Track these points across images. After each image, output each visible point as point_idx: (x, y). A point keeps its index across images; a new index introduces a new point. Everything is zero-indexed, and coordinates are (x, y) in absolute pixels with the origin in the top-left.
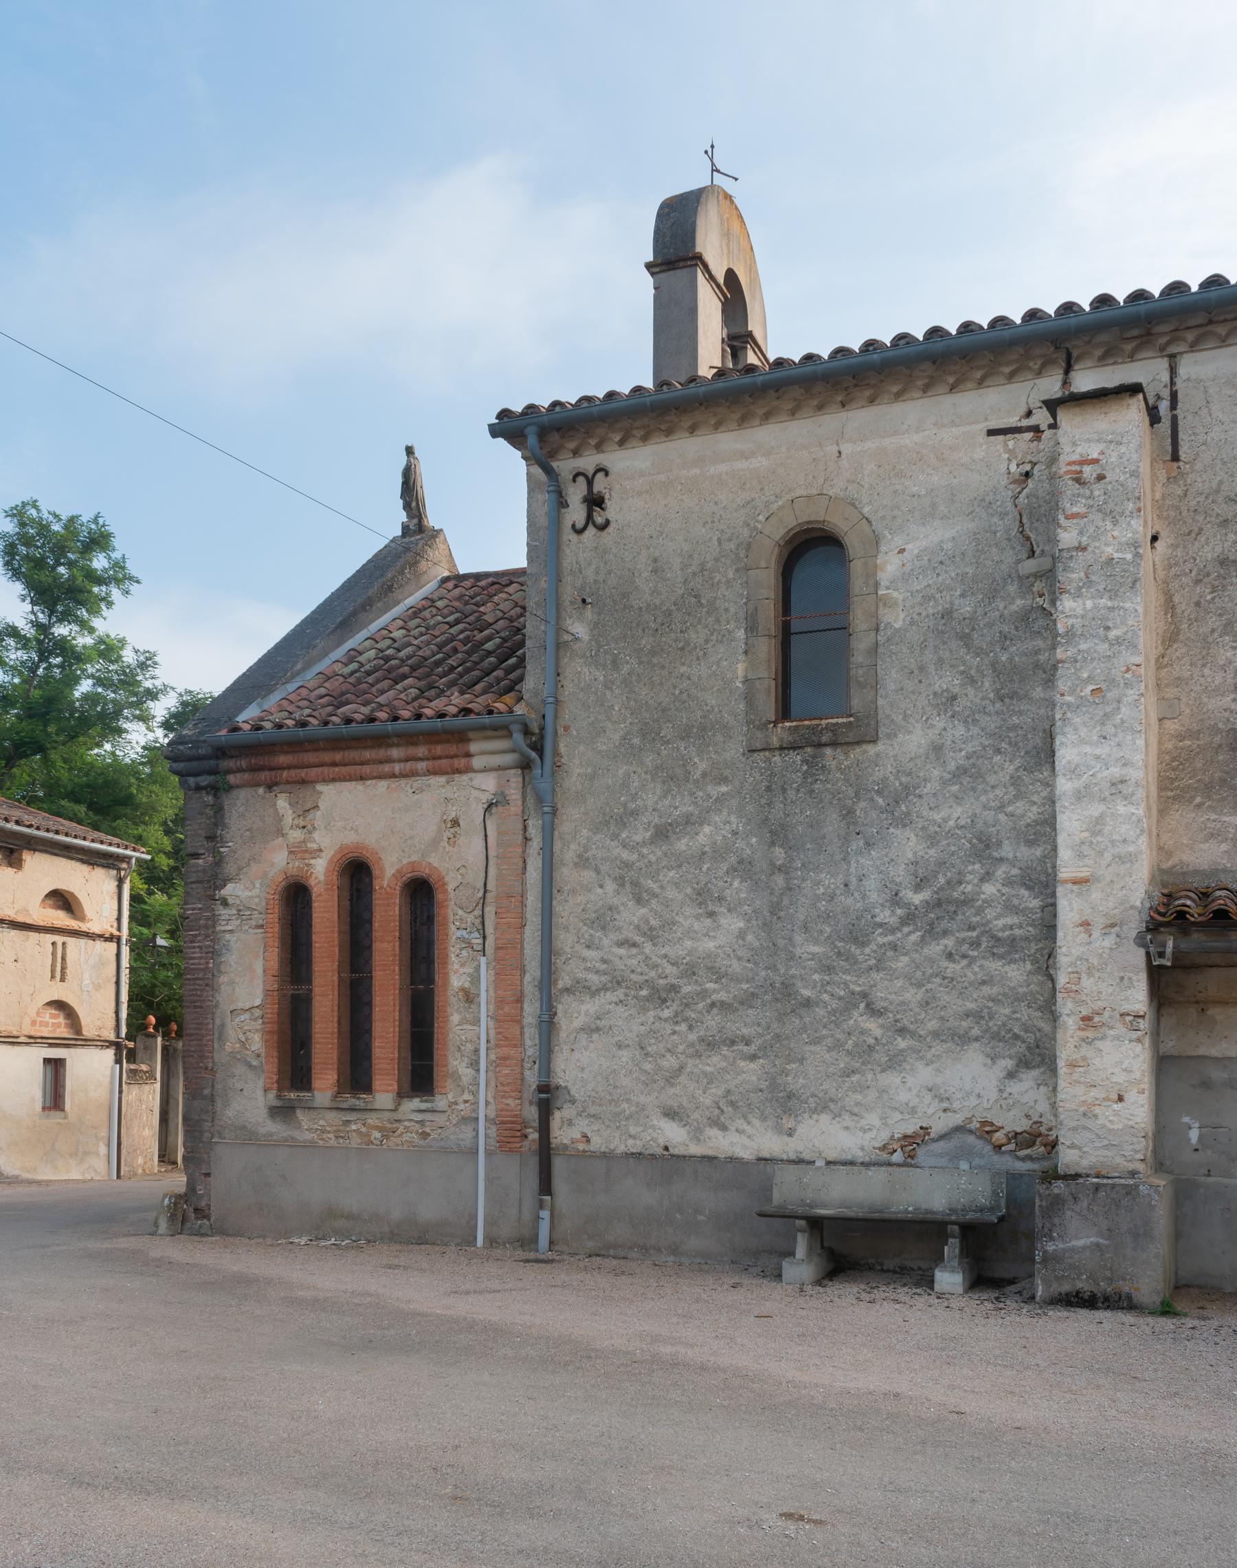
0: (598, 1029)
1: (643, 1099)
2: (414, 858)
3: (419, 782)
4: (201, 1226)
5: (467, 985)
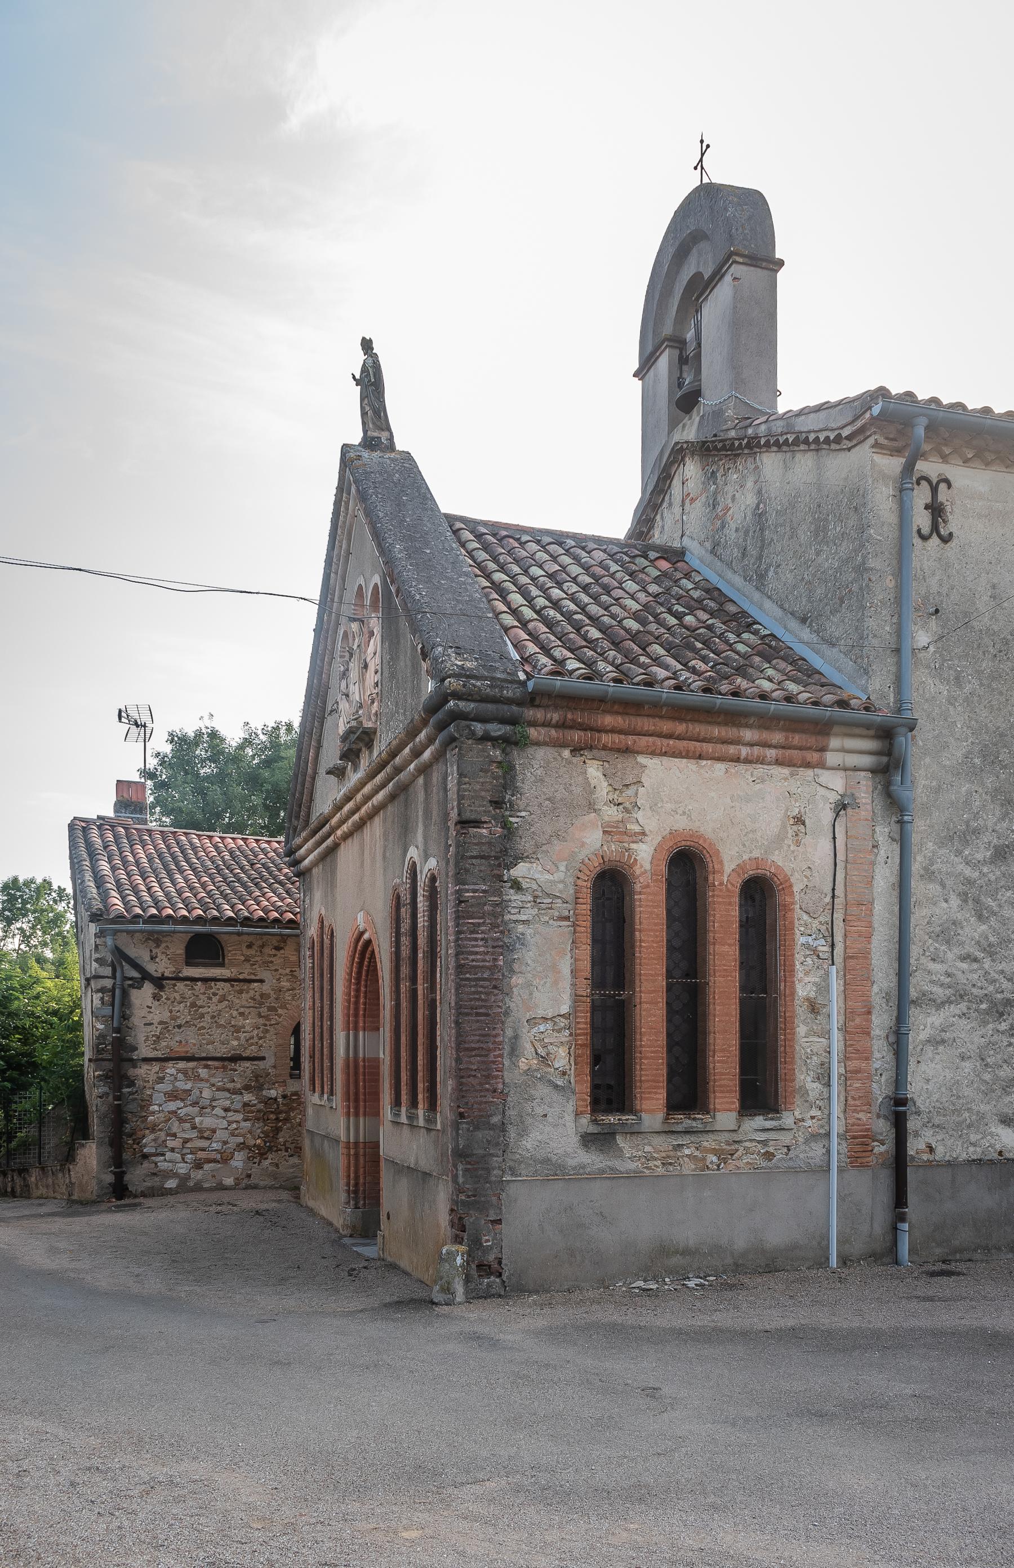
0: (943, 1041)
1: (983, 1108)
2: (756, 854)
3: (760, 770)
4: (489, 1285)
5: (812, 995)
